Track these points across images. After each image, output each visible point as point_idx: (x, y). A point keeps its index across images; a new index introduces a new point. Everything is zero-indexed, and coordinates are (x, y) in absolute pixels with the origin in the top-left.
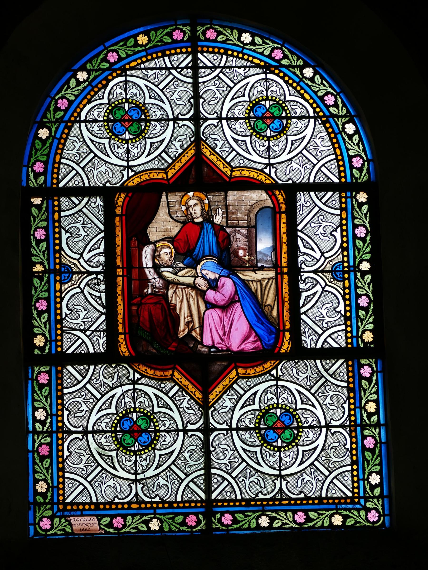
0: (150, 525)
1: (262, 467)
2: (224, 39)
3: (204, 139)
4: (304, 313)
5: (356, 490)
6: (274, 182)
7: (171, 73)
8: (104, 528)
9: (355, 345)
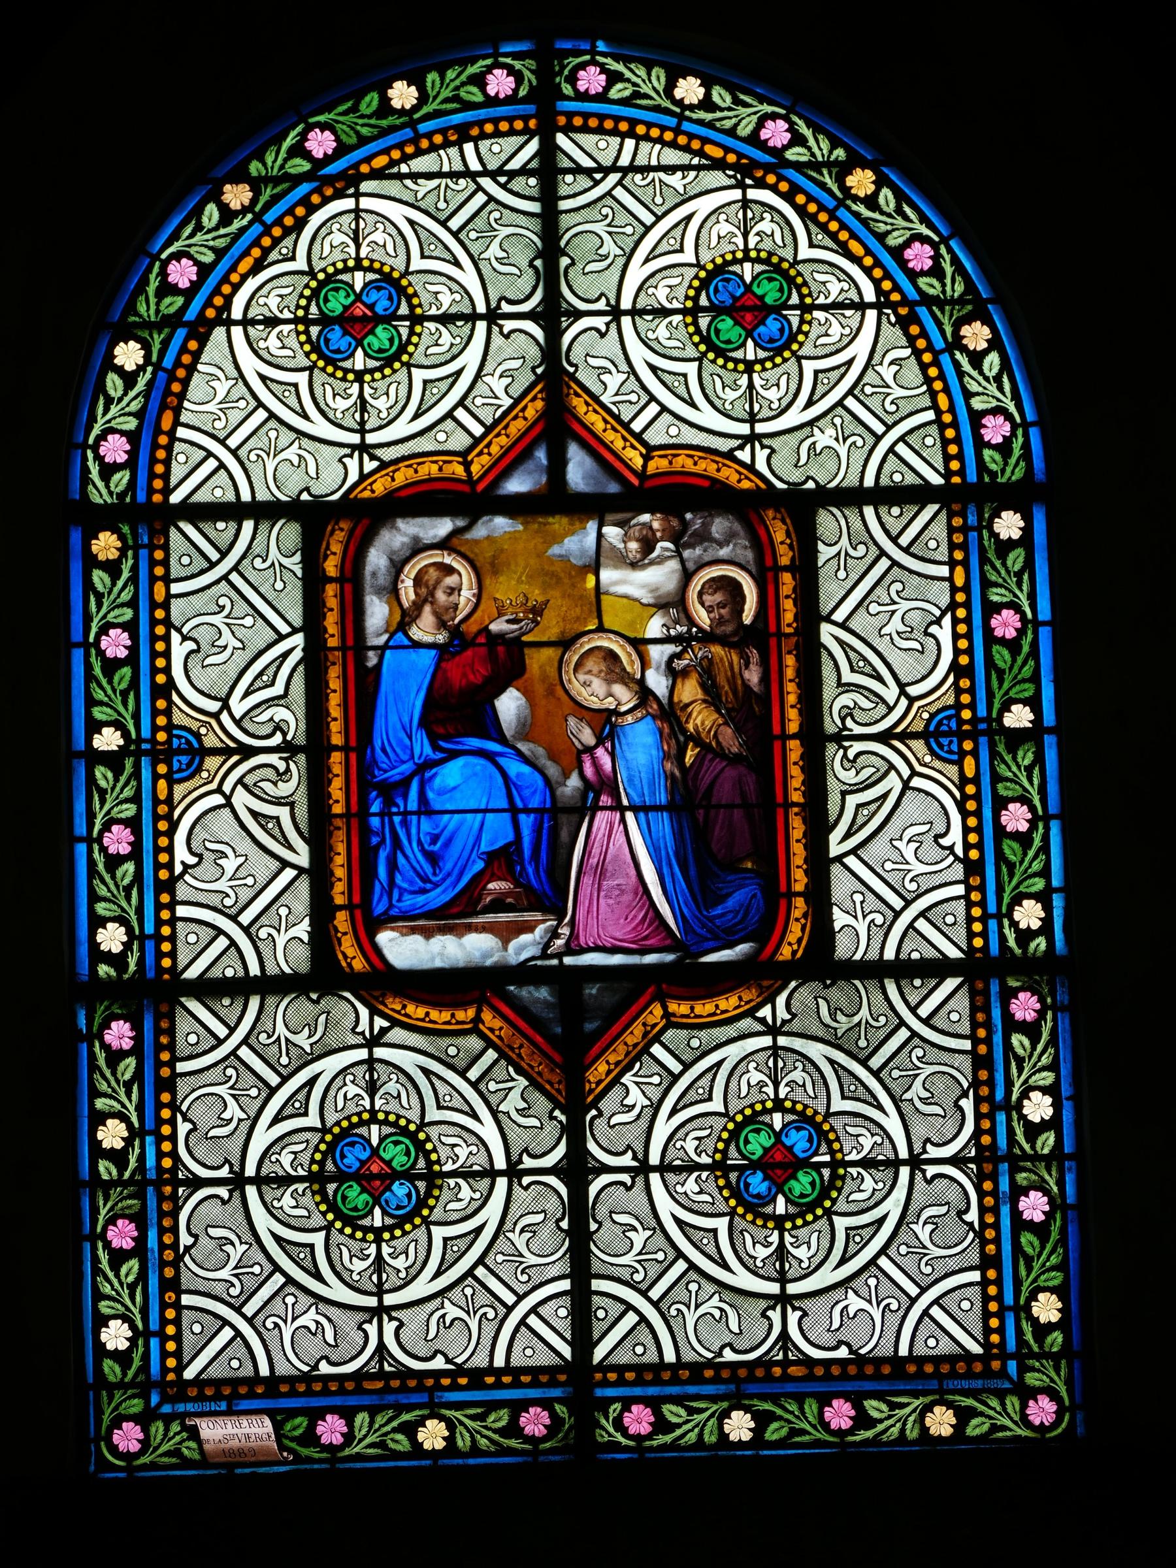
0: (421, 1437)
2: (627, 93)
3: (572, 370)
5: (995, 1338)
6: (763, 486)
7: (480, 188)
8: (293, 1445)
9: (994, 949)
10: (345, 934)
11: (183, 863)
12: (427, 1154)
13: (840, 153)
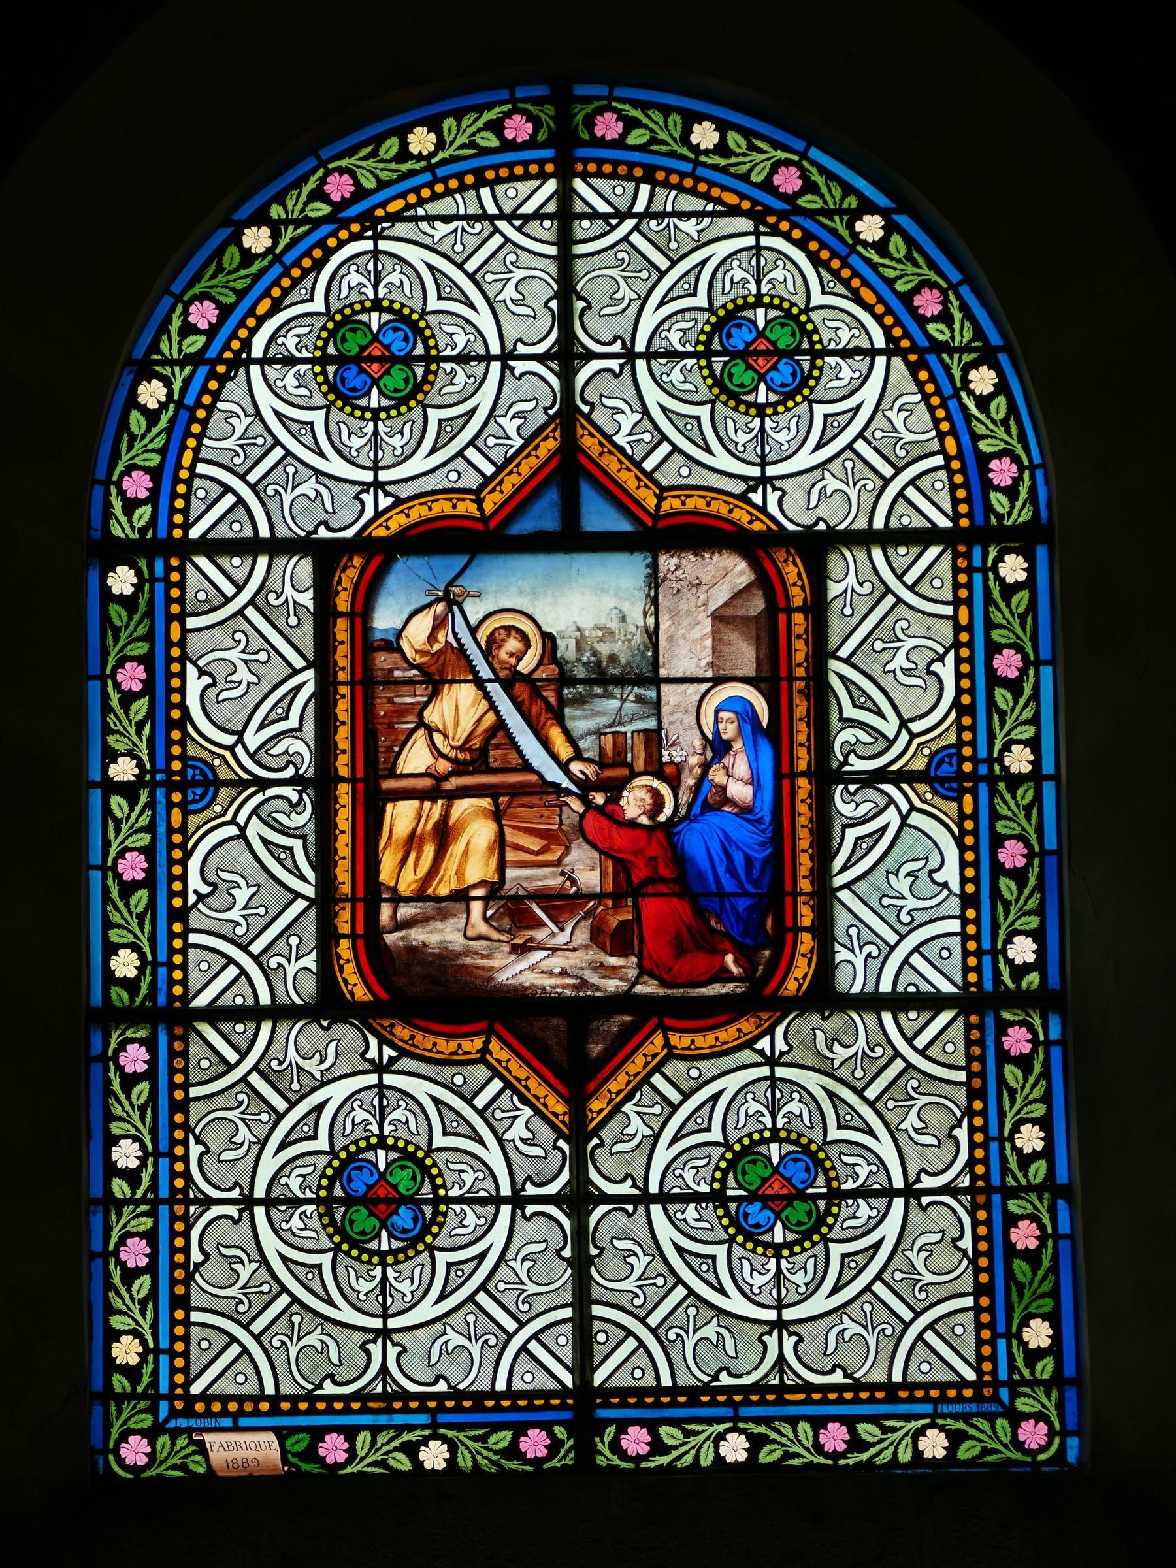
0: (422, 1456)
1: (728, 1296)
3: (586, 409)
4: (848, 886)
6: (774, 527)
7: (496, 230)
9: (988, 986)
10: (348, 961)
11: (196, 892)
12: (432, 1179)
13: (852, 202)
